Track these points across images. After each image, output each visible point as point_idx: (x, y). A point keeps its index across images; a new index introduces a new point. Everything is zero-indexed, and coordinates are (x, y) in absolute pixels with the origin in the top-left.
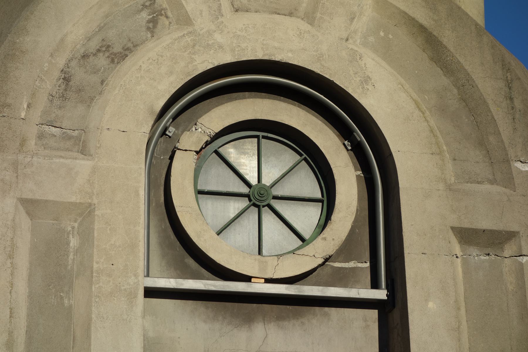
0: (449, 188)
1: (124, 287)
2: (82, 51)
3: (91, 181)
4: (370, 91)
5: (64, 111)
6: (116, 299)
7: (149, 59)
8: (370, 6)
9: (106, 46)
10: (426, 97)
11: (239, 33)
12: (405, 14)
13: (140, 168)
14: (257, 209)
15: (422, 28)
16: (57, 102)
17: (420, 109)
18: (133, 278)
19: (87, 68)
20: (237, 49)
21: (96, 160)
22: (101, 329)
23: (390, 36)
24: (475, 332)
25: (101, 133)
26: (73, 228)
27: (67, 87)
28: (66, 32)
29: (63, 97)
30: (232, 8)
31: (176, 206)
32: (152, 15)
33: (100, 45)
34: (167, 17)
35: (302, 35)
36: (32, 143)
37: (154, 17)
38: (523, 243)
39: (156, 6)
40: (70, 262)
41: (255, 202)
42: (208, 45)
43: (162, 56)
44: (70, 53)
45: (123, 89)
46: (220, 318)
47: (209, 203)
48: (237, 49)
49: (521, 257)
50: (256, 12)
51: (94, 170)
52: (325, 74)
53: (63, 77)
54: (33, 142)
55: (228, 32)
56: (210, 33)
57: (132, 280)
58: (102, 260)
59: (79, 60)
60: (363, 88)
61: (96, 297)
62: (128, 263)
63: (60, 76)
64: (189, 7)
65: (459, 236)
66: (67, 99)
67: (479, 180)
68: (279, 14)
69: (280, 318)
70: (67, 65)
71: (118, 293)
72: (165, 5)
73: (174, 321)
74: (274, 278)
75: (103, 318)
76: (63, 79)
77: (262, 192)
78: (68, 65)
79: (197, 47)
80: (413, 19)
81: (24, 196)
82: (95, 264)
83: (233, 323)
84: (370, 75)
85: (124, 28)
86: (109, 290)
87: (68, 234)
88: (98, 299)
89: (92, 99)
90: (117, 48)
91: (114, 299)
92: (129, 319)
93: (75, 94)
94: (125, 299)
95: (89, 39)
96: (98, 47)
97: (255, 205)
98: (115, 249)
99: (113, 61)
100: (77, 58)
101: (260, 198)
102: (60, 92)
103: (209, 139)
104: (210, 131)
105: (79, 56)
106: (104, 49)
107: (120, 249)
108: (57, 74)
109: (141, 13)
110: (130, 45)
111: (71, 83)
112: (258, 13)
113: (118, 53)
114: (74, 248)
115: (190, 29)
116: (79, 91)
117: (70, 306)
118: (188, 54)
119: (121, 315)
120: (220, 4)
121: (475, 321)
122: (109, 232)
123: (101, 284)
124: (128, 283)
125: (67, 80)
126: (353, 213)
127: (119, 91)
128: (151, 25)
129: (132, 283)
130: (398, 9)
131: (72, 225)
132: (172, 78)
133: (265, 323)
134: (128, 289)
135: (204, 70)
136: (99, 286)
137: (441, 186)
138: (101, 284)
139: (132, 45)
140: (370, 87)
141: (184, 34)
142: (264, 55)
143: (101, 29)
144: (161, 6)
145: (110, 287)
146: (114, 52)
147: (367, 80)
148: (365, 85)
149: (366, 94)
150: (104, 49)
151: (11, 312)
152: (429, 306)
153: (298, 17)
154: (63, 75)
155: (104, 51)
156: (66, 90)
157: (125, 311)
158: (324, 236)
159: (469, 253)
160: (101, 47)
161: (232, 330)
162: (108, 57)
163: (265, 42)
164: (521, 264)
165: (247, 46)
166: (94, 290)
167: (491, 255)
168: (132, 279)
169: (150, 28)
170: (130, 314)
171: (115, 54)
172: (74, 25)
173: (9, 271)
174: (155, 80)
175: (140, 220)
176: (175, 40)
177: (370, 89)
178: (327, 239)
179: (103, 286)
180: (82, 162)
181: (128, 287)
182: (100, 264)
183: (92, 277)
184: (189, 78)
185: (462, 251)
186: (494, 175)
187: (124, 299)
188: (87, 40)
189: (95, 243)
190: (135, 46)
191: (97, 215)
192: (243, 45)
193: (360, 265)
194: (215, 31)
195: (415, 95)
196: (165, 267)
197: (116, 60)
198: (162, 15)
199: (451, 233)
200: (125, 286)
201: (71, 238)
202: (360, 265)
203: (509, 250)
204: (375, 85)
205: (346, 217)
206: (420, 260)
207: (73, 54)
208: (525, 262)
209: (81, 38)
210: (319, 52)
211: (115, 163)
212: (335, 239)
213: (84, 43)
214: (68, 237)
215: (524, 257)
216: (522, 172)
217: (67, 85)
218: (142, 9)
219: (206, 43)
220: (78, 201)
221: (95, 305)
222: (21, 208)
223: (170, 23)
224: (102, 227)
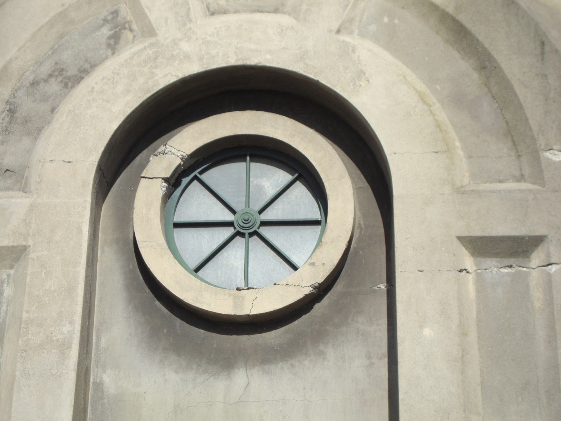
0: (460, 191)
1: (57, 337)
2: (31, 78)
3: (27, 221)
4: (363, 87)
5: (7, 146)
6: (45, 351)
7: (103, 78)
9: (59, 70)
10: (438, 87)
11: (209, 38)
13: (85, 201)
14: (255, 237)
17: (425, 102)
18: (68, 325)
19: (36, 96)
21: (35, 196)
22: (25, 388)
23: (396, 21)
24: (490, 363)
25: (42, 166)
27: (12, 119)
30: (208, 12)
31: (139, 242)
32: (114, 30)
33: (52, 69)
34: (131, 30)
37: (116, 32)
38: (552, 249)
39: (119, 19)
41: (239, 230)
42: (172, 55)
43: (118, 74)
44: (16, 81)
45: (71, 115)
46: (195, 366)
48: (205, 57)
49: (550, 267)
51: (32, 208)
52: (309, 73)
53: (8, 108)
55: (197, 39)
57: (66, 328)
59: (27, 88)
60: (355, 84)
61: (22, 351)
62: (63, 309)
63: (4, 108)
64: (153, 16)
65: (469, 246)
66: (10, 132)
67: (502, 178)
68: (262, 12)
71: (48, 345)
72: (130, 18)
73: (140, 374)
74: (251, 314)
75: (28, 374)
76: (8, 111)
77: (246, 218)
78: (14, 95)
79: (160, 60)
82: (24, 313)
83: (209, 371)
85: (80, 48)
86: (39, 342)
87: (3, 282)
88: (24, 354)
89: (40, 130)
90: (72, 71)
91: (44, 352)
92: (59, 374)
93: (21, 126)
94: (56, 351)
96: (50, 72)
97: (251, 235)
98: (49, 295)
99: (66, 86)
100: (25, 86)
102: (3, 125)
103: (182, 163)
105: (28, 84)
106: (56, 73)
107: (56, 294)
110: (87, 66)
111: (16, 115)
112: (238, 14)
113: (73, 76)
114: (8, 298)
115: (153, 40)
116: (26, 122)
118: (149, 68)
119: (50, 370)
120: (189, 8)
121: (490, 349)
122: (43, 276)
123: (30, 336)
124: (61, 333)
125: (12, 112)
126: (348, 232)
127: (67, 117)
128: (112, 42)
129: (66, 332)
131: (8, 272)
132: (129, 98)
133: (248, 369)
134: (61, 340)
135: (165, 84)
136: (27, 339)
138: (30, 336)
139: (89, 66)
140: (363, 83)
141: (145, 46)
142: (237, 60)
143: (54, 51)
144: (125, 18)
145: (40, 338)
146: (67, 76)
147: (361, 74)
148: (357, 81)
149: (358, 91)
150: (56, 73)
152: (424, 333)
155: (57, 76)
156: (10, 123)
157: (55, 364)
158: (312, 261)
159: (485, 267)
161: (207, 379)
162: (61, 82)
164: (549, 275)
165: (218, 52)
166: (21, 343)
167: (514, 268)
168: (66, 327)
169: (111, 45)
170: (61, 368)
171: (69, 78)
172: (19, 49)
174: (109, 102)
175: (81, 259)
176: (134, 54)
178: (315, 265)
179: (32, 338)
181: (61, 336)
182: (30, 313)
183: (20, 328)
184: (148, 95)
185: (476, 265)
187: (55, 351)
188: (38, 65)
189: (26, 290)
191: (31, 258)
194: (181, 39)
196: (132, 313)
197: (70, 84)
198: (125, 28)
200: (58, 335)
201: (6, 287)
204: (370, 80)
205: (340, 236)
206: (415, 279)
207: (21, 82)
208: (554, 272)
209: (30, 63)
211: (57, 199)
212: (325, 264)
213: (34, 69)
215: (553, 266)
216: (555, 163)
217: (12, 117)
218: (103, 25)
219: (170, 54)
221: (21, 360)
223: (134, 36)
224: (36, 271)
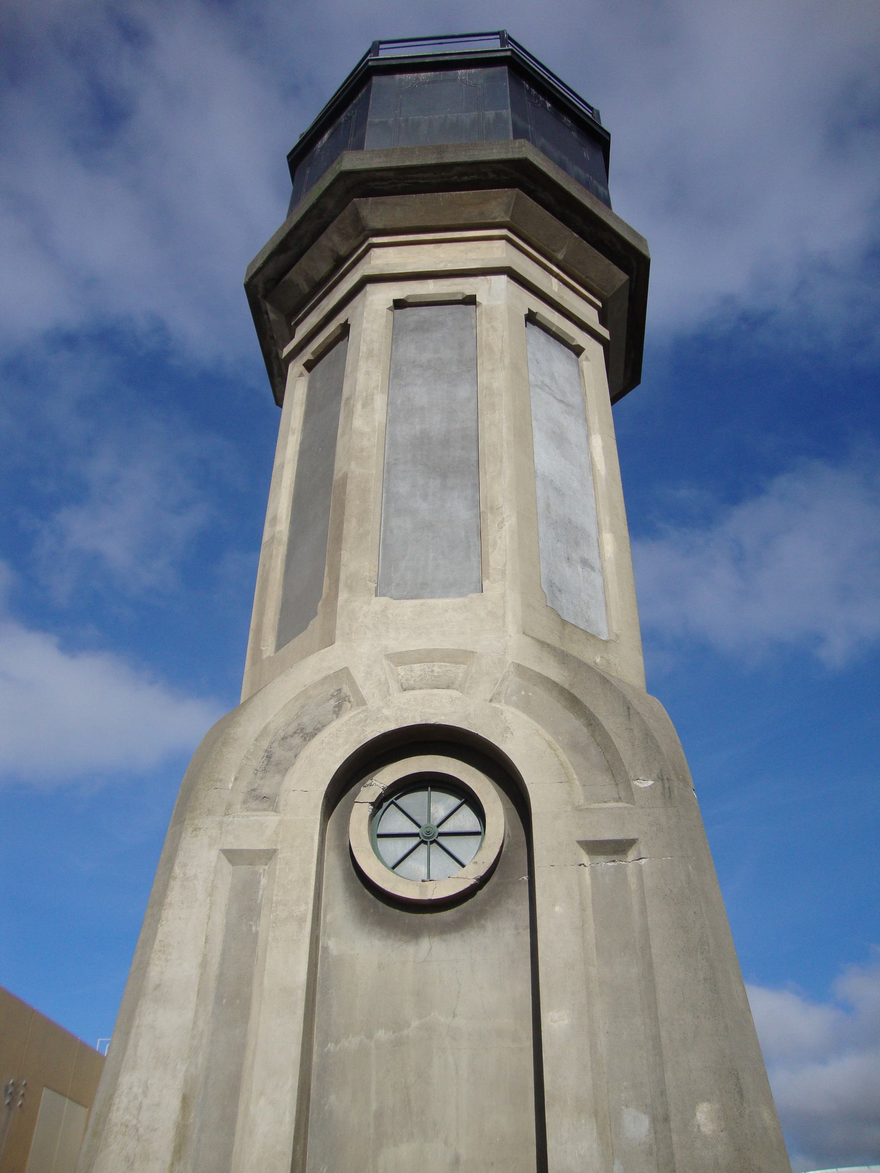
0: (578, 809)
3: (277, 832)
8: (512, 672)
11: (402, 706)
12: (539, 675)
13: (316, 818)
14: (435, 844)
15: (555, 684)
16: (260, 775)
20: (400, 719)
23: (530, 694)
26: (264, 870)
28: (268, 721)
29: (265, 770)
33: (296, 729)
34: (350, 702)
35: (454, 701)
40: (260, 896)
42: (377, 718)
47: (382, 843)
49: (641, 860)
50: (420, 689)
51: (280, 823)
54: (239, 807)
58: (280, 893)
79: (368, 721)
80: (547, 678)
81: (225, 848)
84: (509, 725)
89: (287, 770)
90: (309, 730)
91: (287, 924)
96: (294, 730)
99: (305, 739)
101: (429, 836)
104: (383, 785)
108: (262, 753)
109: (330, 701)
110: (319, 726)
111: (271, 760)
112: (422, 690)
115: (364, 708)
117: (257, 933)
122: (287, 870)
123: (278, 912)
125: (269, 757)
128: (337, 709)
130: (535, 672)
137: (569, 808)
140: (509, 735)
150: (299, 731)
151: (206, 939)
153: (454, 689)
154: (266, 754)
155: (299, 733)
156: (267, 765)
158: (475, 861)
160: (297, 730)
162: (302, 736)
163: (423, 711)
164: (640, 866)
169: (336, 712)
173: (208, 907)
177: (509, 737)
180: (272, 818)
186: (619, 794)
192: (405, 715)
195: (550, 737)
197: (308, 738)
198: (345, 701)
199: (577, 846)
203: (632, 855)
210: (467, 713)
214: (260, 877)
220: (265, 848)
222: (222, 856)
223: (352, 706)
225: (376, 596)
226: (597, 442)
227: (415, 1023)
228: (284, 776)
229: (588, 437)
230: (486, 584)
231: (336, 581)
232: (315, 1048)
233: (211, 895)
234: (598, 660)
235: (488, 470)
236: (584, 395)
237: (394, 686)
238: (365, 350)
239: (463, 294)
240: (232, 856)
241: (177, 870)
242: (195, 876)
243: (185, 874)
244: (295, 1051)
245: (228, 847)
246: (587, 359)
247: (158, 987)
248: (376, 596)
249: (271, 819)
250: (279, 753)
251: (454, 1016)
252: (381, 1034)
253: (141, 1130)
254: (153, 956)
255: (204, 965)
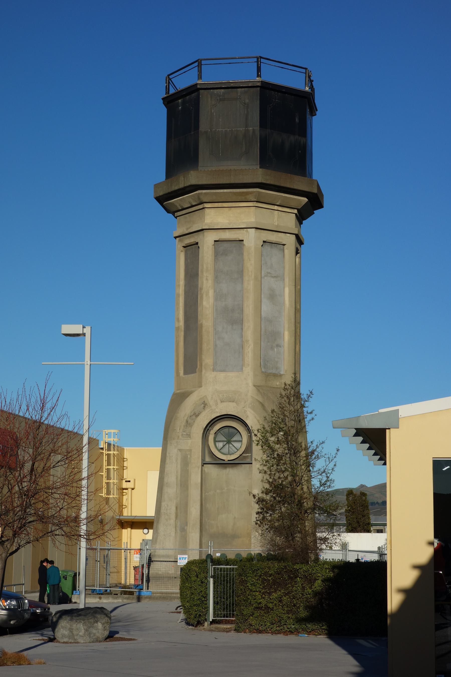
15: (260, 402)
16: (185, 427)
29: (187, 426)
36: (180, 437)
54: (181, 436)
56: (215, 409)
69: (232, 467)
70: (187, 419)
90: (197, 414)
95: (191, 412)
108: (185, 421)
110: (200, 413)
117: (188, 470)
125: (187, 422)
128: (204, 408)
143: (194, 410)
147: (247, 417)
190: (201, 413)
192: (222, 411)
193: (249, 455)
202: (249, 455)
225: (213, 372)
226: (287, 291)
227: (226, 489)
228: (191, 427)
229: (284, 288)
230: (244, 368)
231: (201, 365)
232: (203, 494)
233: (176, 461)
234: (278, 384)
235: (246, 325)
236: (284, 268)
237: (219, 401)
238: (205, 268)
239: (239, 239)
240: (180, 450)
241: (168, 455)
242: (172, 456)
243: (170, 456)
244: (199, 498)
245: (179, 448)
246: (287, 249)
247: (167, 483)
248: (214, 370)
249: (190, 441)
250: (190, 421)
251: (235, 487)
252: (218, 491)
253: (168, 514)
254: (165, 476)
255: (177, 478)
